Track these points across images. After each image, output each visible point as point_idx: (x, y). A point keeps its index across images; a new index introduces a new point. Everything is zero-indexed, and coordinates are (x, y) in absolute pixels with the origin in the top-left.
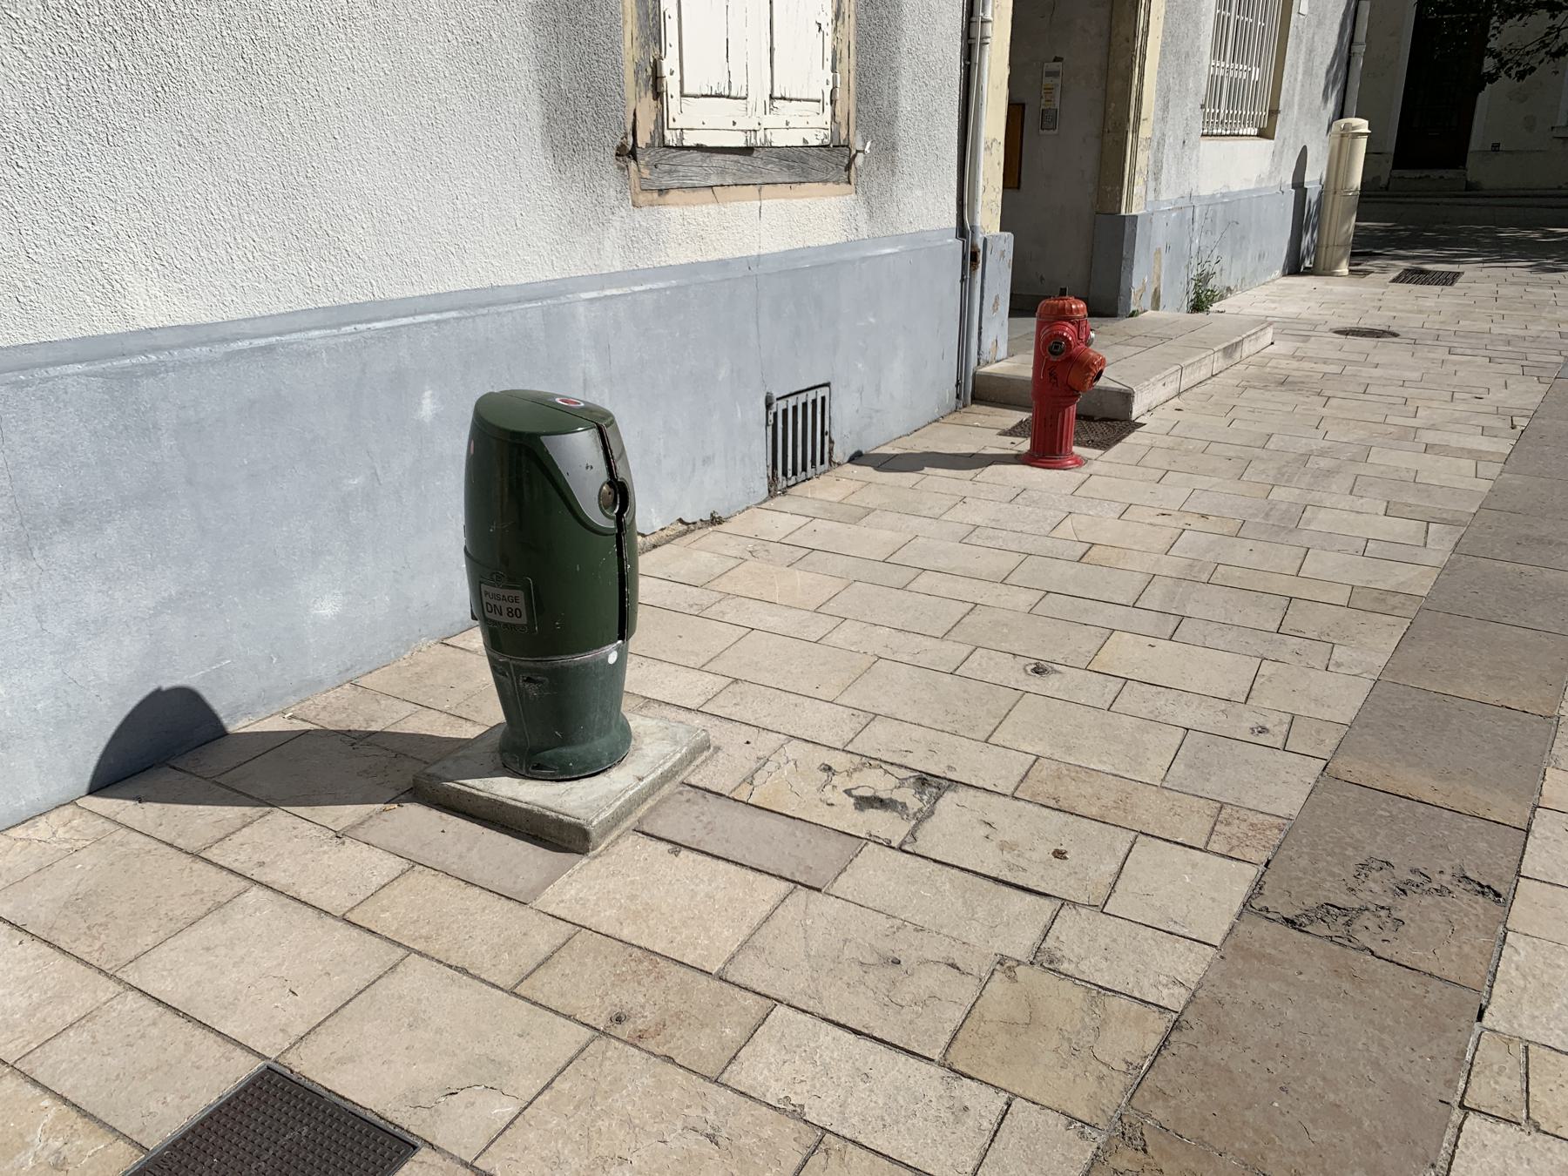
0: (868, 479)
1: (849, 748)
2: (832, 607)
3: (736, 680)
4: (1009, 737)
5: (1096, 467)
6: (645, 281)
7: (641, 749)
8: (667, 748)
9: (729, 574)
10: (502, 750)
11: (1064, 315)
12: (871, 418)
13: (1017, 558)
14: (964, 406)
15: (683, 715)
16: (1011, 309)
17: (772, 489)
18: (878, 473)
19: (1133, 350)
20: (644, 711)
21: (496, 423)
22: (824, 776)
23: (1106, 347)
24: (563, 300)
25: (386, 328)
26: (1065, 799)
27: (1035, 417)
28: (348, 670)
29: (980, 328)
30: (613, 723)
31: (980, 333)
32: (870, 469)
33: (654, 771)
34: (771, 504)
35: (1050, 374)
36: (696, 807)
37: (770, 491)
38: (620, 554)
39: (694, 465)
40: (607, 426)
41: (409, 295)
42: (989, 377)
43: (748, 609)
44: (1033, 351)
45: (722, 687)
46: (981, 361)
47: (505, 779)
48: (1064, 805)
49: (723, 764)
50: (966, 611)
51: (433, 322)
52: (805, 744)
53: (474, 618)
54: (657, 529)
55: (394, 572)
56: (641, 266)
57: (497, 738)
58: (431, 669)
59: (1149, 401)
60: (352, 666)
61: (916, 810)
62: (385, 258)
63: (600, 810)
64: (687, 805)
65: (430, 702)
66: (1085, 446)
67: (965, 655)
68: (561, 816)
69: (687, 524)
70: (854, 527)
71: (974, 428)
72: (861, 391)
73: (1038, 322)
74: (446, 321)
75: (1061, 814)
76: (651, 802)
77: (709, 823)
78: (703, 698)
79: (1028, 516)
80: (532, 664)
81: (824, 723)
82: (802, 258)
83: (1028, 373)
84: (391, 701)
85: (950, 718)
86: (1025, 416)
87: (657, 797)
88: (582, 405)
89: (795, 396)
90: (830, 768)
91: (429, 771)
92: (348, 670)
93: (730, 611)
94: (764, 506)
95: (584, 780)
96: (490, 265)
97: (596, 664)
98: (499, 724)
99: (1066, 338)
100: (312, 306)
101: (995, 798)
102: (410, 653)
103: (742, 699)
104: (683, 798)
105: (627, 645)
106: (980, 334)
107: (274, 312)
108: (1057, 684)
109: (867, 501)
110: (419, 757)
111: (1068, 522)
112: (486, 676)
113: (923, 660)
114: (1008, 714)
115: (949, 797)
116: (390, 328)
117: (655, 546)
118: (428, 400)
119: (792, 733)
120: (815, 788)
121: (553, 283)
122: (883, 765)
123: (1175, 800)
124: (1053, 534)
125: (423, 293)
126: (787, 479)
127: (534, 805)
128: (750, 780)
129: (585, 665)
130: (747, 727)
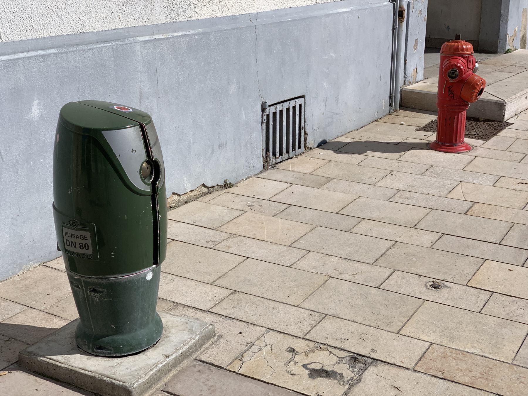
0: (329, 158)
1: (307, 337)
2: (301, 244)
3: (235, 292)
4: (413, 330)
5: (479, 152)
6: (178, 30)
7: (169, 336)
8: (186, 336)
9: (234, 221)
10: (77, 337)
11: (458, 52)
12: (332, 118)
13: (424, 211)
14: (395, 111)
15: (199, 314)
16: (426, 47)
17: (266, 164)
18: (336, 155)
19: (507, 75)
20: (174, 312)
21: (70, 121)
22: (290, 355)
23: (489, 73)
24: (127, 41)
25: (9, 60)
26: (448, 371)
27: (439, 118)
29: (405, 60)
30: (150, 319)
31: (405, 64)
32: (331, 152)
33: (176, 352)
34: (265, 174)
35: (450, 91)
36: (204, 376)
37: (264, 166)
38: (154, 208)
39: (213, 149)
40: (146, 124)
41: (24, 38)
42: (411, 92)
43: (245, 244)
44: (438, 76)
45: (225, 296)
46: (406, 82)
47: (79, 356)
48: (447, 375)
50: (389, 246)
51: (40, 56)
52: (278, 334)
53: (59, 249)
54: (188, 191)
55: (12, 218)
56: (179, 20)
57: (74, 329)
58: (35, 283)
59: (515, 109)
61: (349, 378)
62: (9, 14)
63: (139, 377)
64: (198, 374)
65: (33, 304)
66: (473, 138)
67: (387, 275)
68: (113, 381)
69: (208, 188)
70: (319, 191)
71: (400, 126)
72: (325, 101)
73: (441, 57)
74: (48, 55)
75: (445, 382)
76: (174, 372)
77: (212, 386)
78: (212, 303)
79: (434, 184)
80: (96, 280)
81: (292, 320)
82: (286, 14)
83: (435, 90)
84: (8, 303)
85: (374, 317)
86: (434, 118)
87: (178, 369)
88: (131, 110)
89: (282, 104)
90: (294, 350)
91: (29, 350)
93: (234, 246)
94: (260, 176)
95: (130, 357)
97: (138, 281)
98: (76, 319)
99: (459, 67)
101: (402, 372)
102: (21, 272)
103: (238, 304)
104: (196, 370)
105: (160, 268)
106: (405, 64)
108: (446, 296)
109: (328, 173)
110: (24, 340)
111: (459, 188)
112: (68, 288)
113: (360, 279)
114: (413, 315)
115: (371, 371)
116: (11, 60)
117: (186, 202)
118: (36, 107)
119: (270, 327)
120: (283, 363)
121: (120, 31)
122: (329, 348)
123: (521, 373)
124: (449, 196)
125: (34, 37)
126: (276, 158)
127: (96, 373)
128: (240, 357)
129: (131, 281)
130: (240, 322)
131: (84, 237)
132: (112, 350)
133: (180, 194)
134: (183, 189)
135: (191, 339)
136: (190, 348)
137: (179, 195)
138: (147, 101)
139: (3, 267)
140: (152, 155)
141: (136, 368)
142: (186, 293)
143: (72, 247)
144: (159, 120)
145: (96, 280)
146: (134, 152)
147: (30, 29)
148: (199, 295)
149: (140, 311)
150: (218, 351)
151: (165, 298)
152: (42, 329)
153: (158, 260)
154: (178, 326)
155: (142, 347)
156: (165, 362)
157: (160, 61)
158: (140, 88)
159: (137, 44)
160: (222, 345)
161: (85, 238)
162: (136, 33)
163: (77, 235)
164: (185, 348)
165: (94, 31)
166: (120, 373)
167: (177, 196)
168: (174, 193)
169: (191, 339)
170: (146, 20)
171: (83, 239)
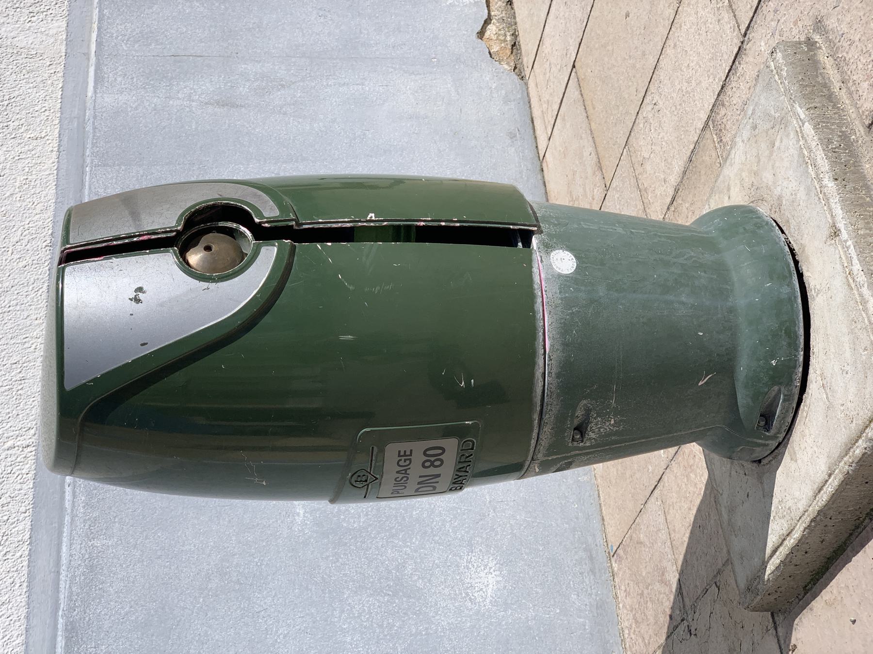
8: (788, 145)
28: (591, 558)
49: (850, 24)
60: (585, 550)
78: (726, 16)
80: (547, 429)
92: (591, 558)
96: (18, 247)
97: (568, 303)
100: (25, 549)
107: (23, 612)
129: (565, 328)
131: (403, 458)
132: (780, 390)
133: (486, 17)
134: (475, 9)
135: (800, 134)
136: (826, 142)
137: (487, 22)
138: (241, 89)
139: (566, 497)
140: (163, 232)
141: (847, 346)
142: (689, 82)
143: (438, 482)
144: (293, 60)
145: (547, 429)
146: (141, 296)
147: (19, 371)
148: (701, 49)
149: (671, 297)
150: (860, 49)
151: (692, 147)
152: (708, 492)
153: (516, 227)
154: (758, 156)
155: (790, 299)
156: (848, 248)
157: (150, 44)
158: (206, 103)
159: (99, 100)
160: (844, 28)
161: (405, 455)
162: (78, 99)
163: (398, 472)
164: (824, 165)
165: (52, 208)
166: (850, 398)
167: (489, 27)
168: (481, 34)
169: (800, 134)
170: (52, 71)
171: (410, 460)
